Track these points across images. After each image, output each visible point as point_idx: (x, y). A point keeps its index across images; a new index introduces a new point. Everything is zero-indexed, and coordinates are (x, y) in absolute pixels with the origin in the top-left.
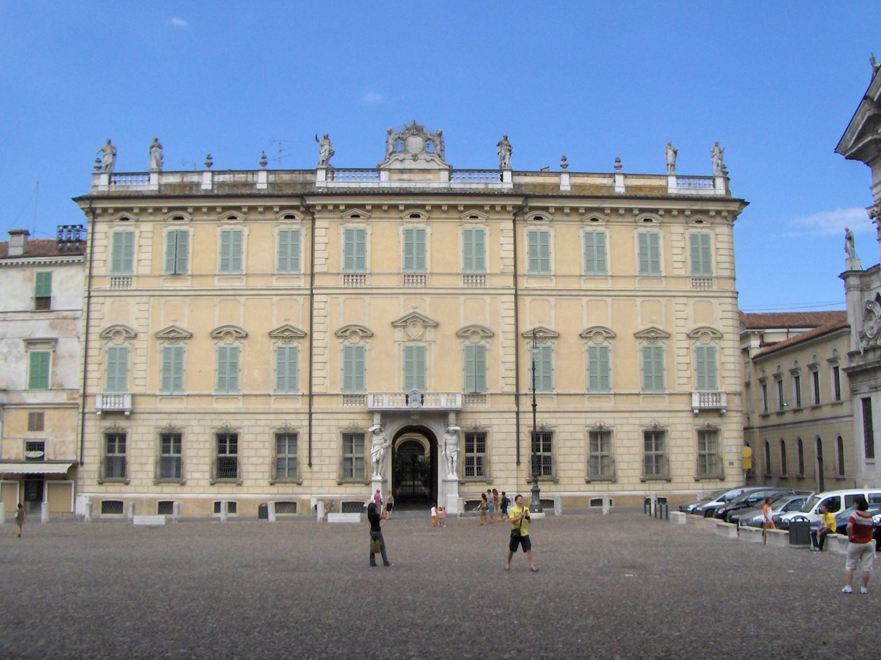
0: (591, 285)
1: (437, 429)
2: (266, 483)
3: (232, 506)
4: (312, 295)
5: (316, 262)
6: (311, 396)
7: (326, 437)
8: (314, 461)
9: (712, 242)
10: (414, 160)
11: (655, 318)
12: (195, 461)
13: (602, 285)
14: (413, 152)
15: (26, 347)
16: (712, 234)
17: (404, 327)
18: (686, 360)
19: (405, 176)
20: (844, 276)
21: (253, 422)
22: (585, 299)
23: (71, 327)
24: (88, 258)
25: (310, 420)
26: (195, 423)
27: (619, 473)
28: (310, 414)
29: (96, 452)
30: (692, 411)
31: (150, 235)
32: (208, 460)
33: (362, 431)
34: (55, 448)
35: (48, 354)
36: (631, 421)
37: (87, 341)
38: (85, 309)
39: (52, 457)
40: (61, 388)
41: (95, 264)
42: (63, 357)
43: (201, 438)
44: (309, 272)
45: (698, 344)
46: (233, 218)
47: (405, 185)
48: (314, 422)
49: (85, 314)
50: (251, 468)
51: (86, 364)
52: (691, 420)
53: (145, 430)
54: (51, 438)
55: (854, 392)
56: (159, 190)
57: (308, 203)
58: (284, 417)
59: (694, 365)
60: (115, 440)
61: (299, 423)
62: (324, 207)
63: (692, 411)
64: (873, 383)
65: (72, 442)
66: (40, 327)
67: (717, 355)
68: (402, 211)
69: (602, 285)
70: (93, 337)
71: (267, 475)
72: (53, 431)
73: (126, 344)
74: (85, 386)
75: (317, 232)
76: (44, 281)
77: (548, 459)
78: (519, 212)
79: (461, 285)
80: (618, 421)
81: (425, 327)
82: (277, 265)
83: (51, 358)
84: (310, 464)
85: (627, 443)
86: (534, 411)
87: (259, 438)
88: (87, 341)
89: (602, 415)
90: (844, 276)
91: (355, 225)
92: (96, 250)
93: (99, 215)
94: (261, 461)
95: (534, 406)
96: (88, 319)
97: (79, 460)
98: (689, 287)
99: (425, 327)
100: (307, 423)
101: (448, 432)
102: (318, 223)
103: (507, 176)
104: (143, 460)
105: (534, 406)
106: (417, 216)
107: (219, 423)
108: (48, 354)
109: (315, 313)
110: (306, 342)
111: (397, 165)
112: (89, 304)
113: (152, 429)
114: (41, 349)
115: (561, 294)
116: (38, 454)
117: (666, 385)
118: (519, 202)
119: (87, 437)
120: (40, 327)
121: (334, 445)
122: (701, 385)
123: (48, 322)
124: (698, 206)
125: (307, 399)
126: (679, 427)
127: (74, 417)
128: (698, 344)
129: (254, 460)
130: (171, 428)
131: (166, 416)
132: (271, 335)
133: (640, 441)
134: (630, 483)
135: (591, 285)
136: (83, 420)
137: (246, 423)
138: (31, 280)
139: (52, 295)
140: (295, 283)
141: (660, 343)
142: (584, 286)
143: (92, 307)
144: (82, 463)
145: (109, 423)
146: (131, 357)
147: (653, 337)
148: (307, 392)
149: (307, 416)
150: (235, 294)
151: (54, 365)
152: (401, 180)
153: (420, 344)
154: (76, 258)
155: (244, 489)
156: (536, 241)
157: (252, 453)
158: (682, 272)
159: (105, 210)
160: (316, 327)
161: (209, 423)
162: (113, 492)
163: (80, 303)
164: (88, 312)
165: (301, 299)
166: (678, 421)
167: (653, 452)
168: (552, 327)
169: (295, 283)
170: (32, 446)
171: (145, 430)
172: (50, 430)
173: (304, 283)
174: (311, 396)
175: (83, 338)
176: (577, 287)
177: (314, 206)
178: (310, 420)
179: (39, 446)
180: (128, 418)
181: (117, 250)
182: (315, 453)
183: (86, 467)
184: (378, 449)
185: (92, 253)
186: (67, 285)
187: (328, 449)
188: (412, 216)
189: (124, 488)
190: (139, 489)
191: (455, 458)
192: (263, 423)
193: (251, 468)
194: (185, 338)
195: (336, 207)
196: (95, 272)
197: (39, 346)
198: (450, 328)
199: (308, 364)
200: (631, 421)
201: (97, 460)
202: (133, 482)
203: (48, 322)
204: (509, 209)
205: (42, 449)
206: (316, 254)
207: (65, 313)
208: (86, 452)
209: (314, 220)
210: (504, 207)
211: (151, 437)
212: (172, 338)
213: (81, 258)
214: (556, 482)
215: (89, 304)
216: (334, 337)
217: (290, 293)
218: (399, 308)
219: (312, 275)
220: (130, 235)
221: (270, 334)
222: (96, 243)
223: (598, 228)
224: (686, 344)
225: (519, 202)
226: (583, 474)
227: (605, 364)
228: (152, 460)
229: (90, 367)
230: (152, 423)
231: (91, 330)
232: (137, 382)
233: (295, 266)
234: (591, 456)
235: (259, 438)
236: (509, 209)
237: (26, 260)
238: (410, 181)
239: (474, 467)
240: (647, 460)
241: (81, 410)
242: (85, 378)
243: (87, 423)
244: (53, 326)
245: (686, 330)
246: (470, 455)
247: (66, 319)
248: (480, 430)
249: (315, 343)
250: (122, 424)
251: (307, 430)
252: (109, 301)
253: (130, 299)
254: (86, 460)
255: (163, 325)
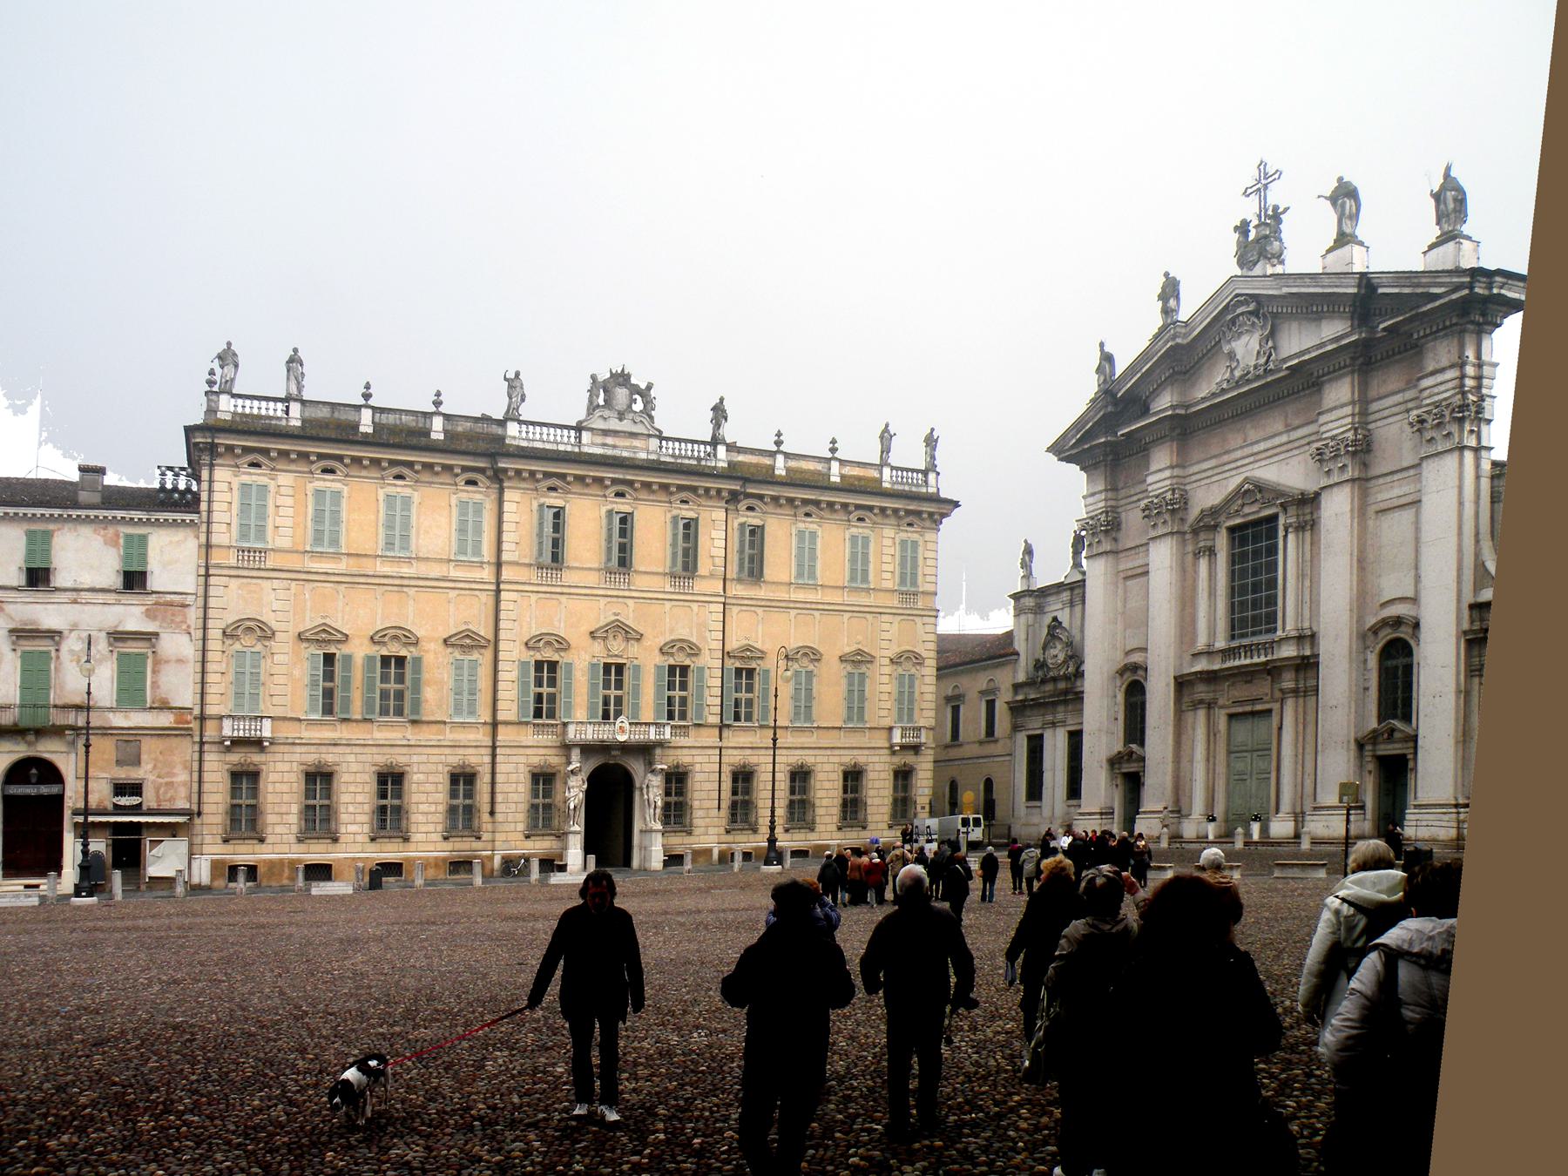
0: (800, 596)
1: (636, 767)
2: (437, 837)
3: (252, 871)
4: (498, 591)
5: (505, 546)
6: (495, 724)
7: (513, 777)
8: (499, 808)
9: (920, 549)
10: (621, 420)
11: (860, 638)
12: (351, 809)
13: (811, 596)
14: (619, 407)
15: (110, 645)
16: (272, 485)
17: (604, 639)
18: (887, 688)
19: (610, 440)
20: (1016, 597)
21: (424, 758)
22: (793, 612)
23: (178, 619)
24: (204, 518)
25: (494, 756)
26: (351, 758)
27: (870, 818)
28: (494, 747)
29: (218, 798)
30: (222, 743)
31: (291, 492)
32: (367, 808)
33: (329, 770)
34: (157, 793)
35: (48, 653)
36: (832, 759)
37: (204, 639)
38: (201, 591)
39: (154, 805)
40: (164, 706)
41: (215, 527)
42: (167, 662)
43: (360, 778)
44: (493, 560)
45: (900, 670)
46: (399, 477)
47: (610, 452)
48: (499, 759)
49: (201, 602)
50: (421, 818)
51: (203, 672)
52: (888, 759)
53: (286, 767)
54: (151, 777)
55: (1016, 728)
56: (303, 427)
57: (500, 465)
58: (461, 751)
59: (895, 695)
60: (245, 779)
61: (478, 759)
62: (518, 472)
63: (892, 746)
64: (1049, 718)
65: (184, 784)
66: (131, 615)
67: (917, 683)
68: (238, 456)
69: (811, 596)
70: (215, 634)
71: (440, 828)
72: (155, 767)
73: (259, 647)
74: (202, 704)
75: (507, 507)
76: (39, 543)
77: (398, 810)
78: (734, 497)
79: (896, 603)
80: (819, 759)
81: (628, 639)
82: (454, 548)
83: (150, 662)
84: (492, 813)
85: (827, 785)
86: (774, 748)
87: (431, 779)
88: (204, 639)
89: (855, 752)
90: (1016, 597)
91: (400, 489)
92: (215, 506)
93: (220, 455)
94: (433, 808)
95: (775, 740)
96: (205, 608)
97: (195, 808)
98: (896, 603)
99: (628, 639)
100: (487, 759)
101: (653, 771)
102: (508, 495)
103: (721, 450)
104: (284, 810)
105: (775, 740)
106: (332, 471)
107: (382, 758)
108: (145, 656)
109: (503, 615)
110: (489, 653)
111: (600, 425)
112: (206, 585)
113: (522, 768)
114: (133, 648)
115: (769, 605)
116: (134, 800)
117: (814, 716)
118: (736, 486)
119: (207, 777)
120: (131, 615)
121: (521, 788)
122: (900, 719)
123: (143, 609)
124: (912, 507)
125: (489, 729)
126: (878, 767)
127: (187, 749)
128: (900, 670)
129: (423, 808)
130: (320, 764)
131: (313, 749)
132: (842, 659)
133: (372, 786)
134: (355, 843)
135: (800, 596)
136: (201, 752)
137: (698, 759)
138: (115, 544)
139: (149, 568)
140: (477, 574)
141: (863, 669)
142: (793, 597)
143: (212, 591)
144: (199, 814)
145: (235, 757)
146: (265, 665)
147: (858, 660)
148: (489, 720)
149: (489, 751)
150: (401, 584)
151: (154, 672)
152: (604, 445)
153: (620, 661)
154: (188, 517)
155: (412, 846)
156: (466, 514)
157: (423, 798)
158: (889, 585)
159: (230, 449)
160: (502, 635)
161: (369, 758)
162: (244, 854)
163: (188, 582)
164: (206, 597)
165: (483, 597)
166: (876, 759)
167: (460, 801)
168: (759, 645)
169: (477, 574)
170: (120, 789)
171: (286, 767)
172: (150, 767)
173: (487, 574)
174: (775, 728)
175: (200, 634)
176: (786, 596)
177: (505, 470)
178: (494, 756)
179: (136, 789)
180: (262, 749)
181: (245, 507)
182: (499, 798)
183: (206, 819)
184: (575, 792)
185: (209, 512)
186: (172, 556)
187: (514, 794)
188: (325, 471)
189: (258, 847)
190: (278, 848)
191: (659, 803)
192: (434, 759)
193: (421, 818)
194: (339, 641)
195: (532, 474)
196: (215, 540)
197: (130, 643)
198: (654, 640)
199: (490, 683)
200: (832, 759)
201: (221, 808)
202: (270, 839)
203: (143, 609)
204: (725, 494)
205: (140, 794)
206: (505, 537)
207: (169, 598)
208: (205, 798)
209: (501, 491)
210: (719, 491)
211: (293, 777)
212: (324, 641)
213: (194, 517)
214: (690, 833)
215: (206, 585)
216: (523, 648)
217: (470, 587)
218: (599, 613)
219: (499, 565)
220: (263, 488)
221: (445, 641)
222: (216, 497)
223: (810, 525)
224: (887, 670)
225: (736, 486)
226: (521, 827)
227: (809, 690)
228: (295, 809)
229: (210, 678)
230: (297, 757)
231: (210, 623)
232: (276, 700)
233: (477, 551)
234: (307, 806)
235: (431, 779)
236: (725, 494)
237: (102, 513)
238: (614, 447)
239: (676, 813)
240: (845, 804)
241: (197, 739)
242: (203, 694)
243: (207, 757)
244: (150, 614)
245: (890, 654)
246: (384, 802)
247: (168, 606)
248: (468, 770)
249: (502, 656)
250: (256, 758)
251: (488, 768)
252: (234, 583)
253: (266, 584)
254: (206, 809)
255: (309, 622)
